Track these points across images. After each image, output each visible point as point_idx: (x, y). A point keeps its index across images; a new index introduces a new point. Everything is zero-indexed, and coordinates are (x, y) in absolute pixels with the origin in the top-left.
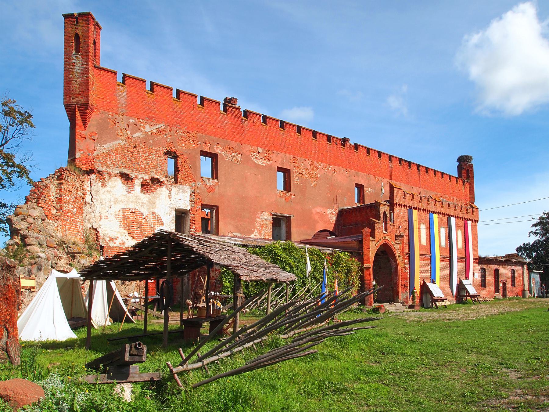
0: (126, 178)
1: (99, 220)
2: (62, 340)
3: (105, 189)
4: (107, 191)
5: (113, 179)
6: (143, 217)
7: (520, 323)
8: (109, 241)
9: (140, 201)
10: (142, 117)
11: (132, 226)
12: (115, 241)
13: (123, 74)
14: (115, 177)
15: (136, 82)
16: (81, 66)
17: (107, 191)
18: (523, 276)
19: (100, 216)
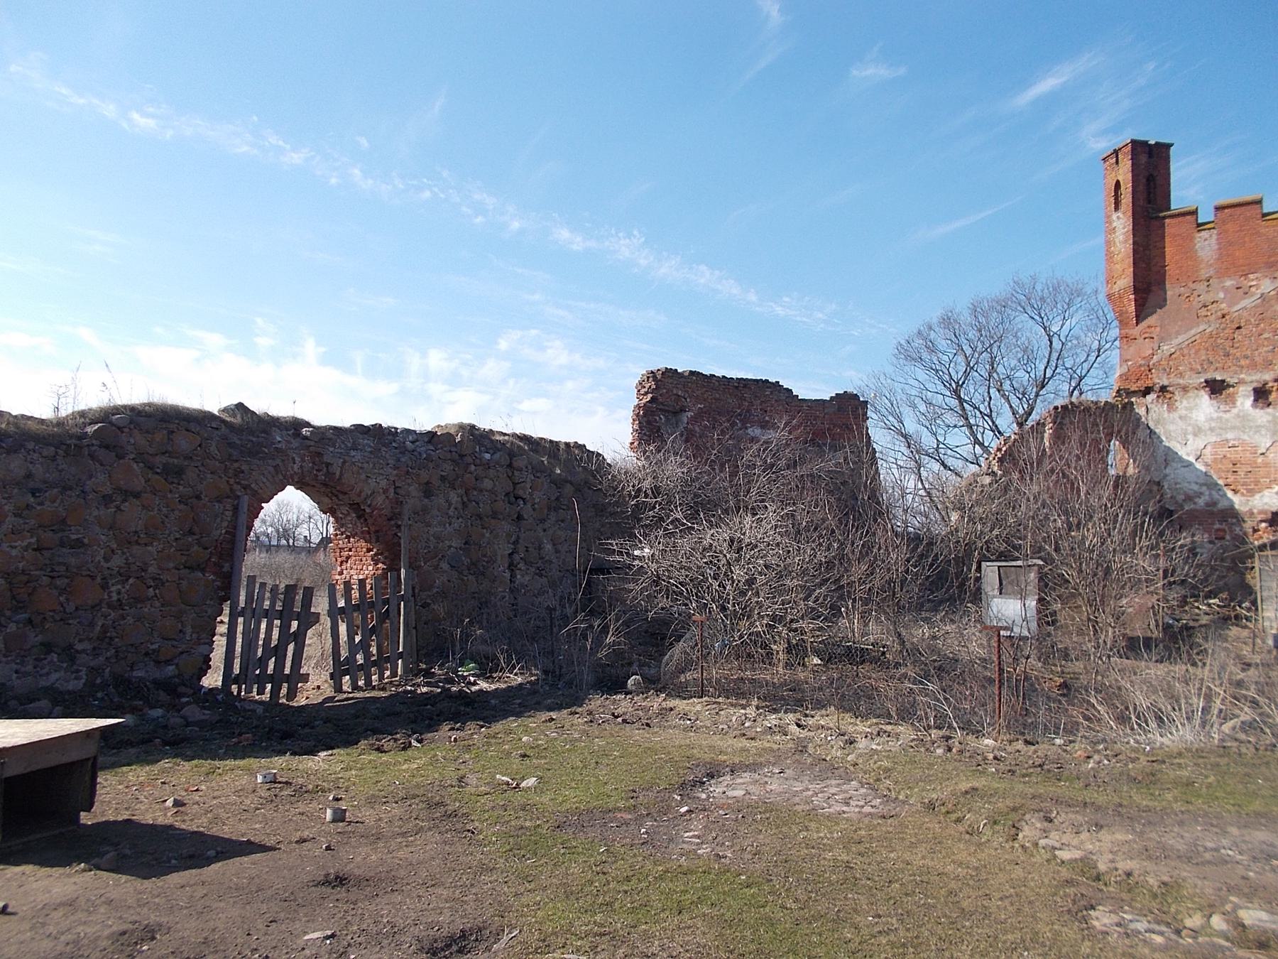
0: (1216, 388)
1: (1163, 467)
2: (280, 415)
3: (1175, 415)
4: (1180, 418)
5: (1190, 394)
6: (1260, 452)
7: (1242, 434)
8: (1184, 500)
9: (1252, 424)
10: (1252, 270)
11: (1234, 472)
12: (1196, 500)
13: (1197, 209)
14: (1196, 391)
15: (1238, 210)
16: (1124, 228)
17: (1180, 418)
18: (1269, 220)
19: (1165, 460)
